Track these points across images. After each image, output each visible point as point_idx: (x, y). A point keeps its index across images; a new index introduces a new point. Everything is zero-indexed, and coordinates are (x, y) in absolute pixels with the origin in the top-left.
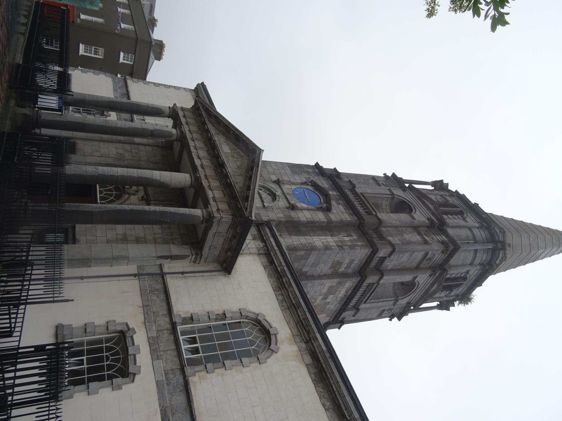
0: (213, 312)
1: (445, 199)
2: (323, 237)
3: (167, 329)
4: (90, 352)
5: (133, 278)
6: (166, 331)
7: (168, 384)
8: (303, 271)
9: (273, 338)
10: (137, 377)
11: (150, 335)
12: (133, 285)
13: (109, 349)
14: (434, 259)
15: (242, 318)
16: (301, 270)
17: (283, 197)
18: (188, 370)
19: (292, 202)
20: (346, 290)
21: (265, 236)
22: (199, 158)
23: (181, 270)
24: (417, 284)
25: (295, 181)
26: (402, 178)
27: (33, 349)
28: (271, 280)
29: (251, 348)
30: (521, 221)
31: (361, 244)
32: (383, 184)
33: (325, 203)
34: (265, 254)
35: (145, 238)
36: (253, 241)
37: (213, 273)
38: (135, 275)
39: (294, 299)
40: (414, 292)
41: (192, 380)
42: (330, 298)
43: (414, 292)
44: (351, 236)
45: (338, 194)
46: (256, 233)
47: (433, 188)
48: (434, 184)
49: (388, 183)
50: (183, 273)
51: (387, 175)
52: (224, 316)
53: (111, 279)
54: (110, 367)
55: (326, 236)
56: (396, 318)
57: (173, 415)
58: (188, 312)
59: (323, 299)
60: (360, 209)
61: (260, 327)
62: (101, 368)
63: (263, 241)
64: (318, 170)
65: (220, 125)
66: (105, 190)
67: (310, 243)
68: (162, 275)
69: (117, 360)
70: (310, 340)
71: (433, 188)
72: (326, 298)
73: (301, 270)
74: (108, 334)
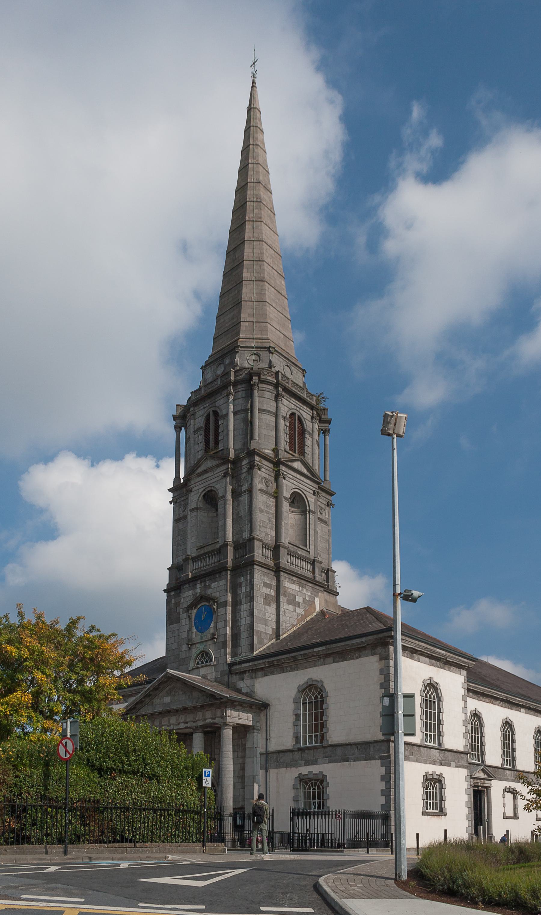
0: (294, 723)
2: (242, 613)
3: (302, 754)
4: (309, 798)
5: (268, 773)
6: (303, 755)
7: (331, 757)
9: (314, 683)
10: (324, 773)
11: (304, 765)
12: (272, 772)
13: (309, 788)
14: (267, 476)
15: (299, 701)
16: (271, 635)
17: (204, 644)
18: (325, 744)
19: (210, 636)
20: (292, 583)
22: (179, 724)
23: (265, 740)
24: (294, 490)
25: (188, 626)
26: (174, 479)
27: (292, 822)
29: (319, 700)
31: (249, 576)
32: (184, 511)
34: (255, 672)
35: (241, 764)
36: (244, 681)
37: (268, 718)
38: (266, 772)
39: (290, 660)
41: (330, 743)
42: (299, 599)
44: (241, 583)
45: (199, 582)
46: (237, 676)
47: (183, 428)
48: (178, 429)
50: (267, 740)
51: (171, 499)
52: (297, 716)
53: (268, 786)
54: (319, 788)
55: (240, 610)
57: (346, 755)
58: (293, 739)
59: (299, 607)
62: (319, 793)
63: (244, 672)
64: (172, 591)
65: (143, 701)
66: (312, 787)
67: (247, 629)
68: (267, 754)
69: (316, 783)
70: (318, 656)
71: (183, 428)
72: (299, 603)
74: (301, 789)
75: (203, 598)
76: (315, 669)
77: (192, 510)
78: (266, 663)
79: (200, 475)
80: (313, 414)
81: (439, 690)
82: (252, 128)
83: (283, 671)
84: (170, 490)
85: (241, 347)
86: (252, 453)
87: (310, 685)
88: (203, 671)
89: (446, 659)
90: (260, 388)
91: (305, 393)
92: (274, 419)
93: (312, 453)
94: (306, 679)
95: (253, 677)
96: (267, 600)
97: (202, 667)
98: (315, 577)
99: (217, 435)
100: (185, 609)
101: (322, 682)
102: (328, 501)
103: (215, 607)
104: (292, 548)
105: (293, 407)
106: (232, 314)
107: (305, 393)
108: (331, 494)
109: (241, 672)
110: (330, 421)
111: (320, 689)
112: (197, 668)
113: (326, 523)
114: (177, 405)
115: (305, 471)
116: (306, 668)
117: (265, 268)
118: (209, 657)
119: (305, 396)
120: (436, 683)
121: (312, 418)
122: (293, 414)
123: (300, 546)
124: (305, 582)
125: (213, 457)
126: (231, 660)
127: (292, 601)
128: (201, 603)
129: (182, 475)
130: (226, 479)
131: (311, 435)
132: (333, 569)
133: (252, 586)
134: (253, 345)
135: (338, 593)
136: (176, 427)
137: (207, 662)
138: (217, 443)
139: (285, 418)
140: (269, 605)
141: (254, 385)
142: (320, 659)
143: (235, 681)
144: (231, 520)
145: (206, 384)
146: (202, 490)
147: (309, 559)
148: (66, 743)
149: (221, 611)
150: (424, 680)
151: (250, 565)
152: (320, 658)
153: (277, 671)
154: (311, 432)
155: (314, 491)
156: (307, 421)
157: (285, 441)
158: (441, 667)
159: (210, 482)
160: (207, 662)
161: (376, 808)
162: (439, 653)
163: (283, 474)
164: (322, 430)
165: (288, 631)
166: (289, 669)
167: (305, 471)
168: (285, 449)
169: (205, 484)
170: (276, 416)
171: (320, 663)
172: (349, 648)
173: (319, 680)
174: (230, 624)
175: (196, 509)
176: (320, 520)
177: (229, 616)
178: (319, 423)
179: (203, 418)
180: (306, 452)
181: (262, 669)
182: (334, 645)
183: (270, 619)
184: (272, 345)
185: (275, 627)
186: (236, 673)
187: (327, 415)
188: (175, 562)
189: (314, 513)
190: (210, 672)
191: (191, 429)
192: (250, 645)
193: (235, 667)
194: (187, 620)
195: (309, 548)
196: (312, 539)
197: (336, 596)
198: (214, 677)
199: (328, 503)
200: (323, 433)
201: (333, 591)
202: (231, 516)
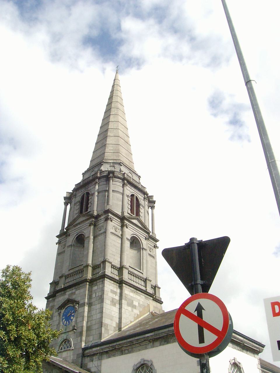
1: (77, 202)
8: (115, 326)
16: (115, 327)
17: (67, 334)
19: (71, 328)
21: (91, 353)
25: (58, 321)
26: (60, 230)
28: (117, 355)
30: (96, 144)
33: (74, 303)
34: (102, 355)
36: (93, 362)
40: (137, 236)
42: (136, 303)
43: (137, 236)
47: (69, 204)
48: (66, 204)
49: (64, 243)
56: (157, 243)
59: (135, 308)
60: (79, 276)
61: (140, 368)
63: (94, 355)
64: (51, 298)
70: (149, 340)
71: (69, 204)
72: (135, 306)
73: (115, 327)
75: (69, 301)
76: (147, 351)
77: (68, 247)
78: (110, 347)
79: (74, 226)
80: (145, 196)
81: (242, 369)
82: (115, 85)
83: (122, 353)
84: (57, 237)
85: (104, 162)
86: (108, 211)
87: (142, 365)
88: (64, 354)
89: (244, 344)
90: (114, 180)
91: (140, 185)
92: (121, 196)
93: (145, 217)
94: (139, 360)
95: (100, 359)
96: (113, 302)
97: (64, 351)
98: (146, 289)
99: (87, 204)
100: (57, 310)
101: (151, 361)
102: (155, 244)
103: (77, 307)
104: (130, 269)
105: (133, 191)
106: (101, 150)
107: (140, 185)
108: (157, 241)
109: (91, 355)
110: (155, 202)
111: (150, 367)
112: (61, 352)
113: (154, 257)
114: (67, 192)
115: (140, 225)
116: (139, 350)
117: (119, 131)
118: (70, 344)
119: (140, 187)
120: (239, 363)
121: (144, 198)
122: (132, 196)
123: (137, 269)
124: (140, 293)
125: (84, 216)
126: (85, 345)
127: (131, 304)
128: (68, 305)
129: (66, 225)
130: (91, 227)
131: (144, 207)
132: (159, 286)
133: (103, 291)
134: (111, 162)
135: (162, 302)
136: (65, 203)
137: (68, 347)
138: (87, 208)
139: (128, 196)
140: (114, 305)
141: (110, 177)
142: (150, 343)
143: (87, 362)
144: (92, 251)
145: (83, 181)
146: (76, 234)
147: (142, 278)
148: (199, 309)
149: (80, 310)
150: (230, 359)
151: (102, 278)
152: (150, 342)
153: (118, 353)
154: (144, 206)
155: (146, 237)
156: (141, 200)
157: (128, 204)
158: (240, 350)
159: (81, 230)
160: (68, 347)
161: (113, 182)
162: (238, 339)
163: (126, 225)
164: (150, 206)
165: (127, 325)
166: (126, 352)
167: (140, 225)
168: (128, 212)
169: (78, 231)
170: (123, 194)
171: (150, 346)
172: (171, 333)
173: (149, 360)
174: (86, 319)
175: (71, 245)
176: (150, 255)
177: (86, 314)
178: (149, 203)
179: (81, 197)
180: (141, 215)
181: (107, 352)
182: (161, 331)
183: (114, 316)
184: (121, 162)
185: (118, 322)
186: (88, 356)
187: (153, 199)
188: (120, 354)
189: (146, 250)
190: (69, 355)
191: (73, 203)
192: (99, 334)
193: (87, 351)
194: (58, 316)
195: (143, 271)
196: (145, 266)
197: (161, 304)
198: (71, 359)
199: (154, 245)
200: (151, 208)
201: (158, 300)
202: (92, 249)
